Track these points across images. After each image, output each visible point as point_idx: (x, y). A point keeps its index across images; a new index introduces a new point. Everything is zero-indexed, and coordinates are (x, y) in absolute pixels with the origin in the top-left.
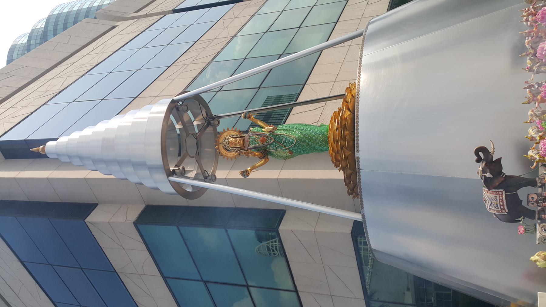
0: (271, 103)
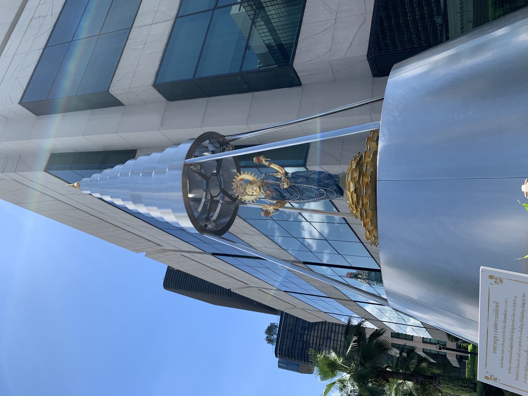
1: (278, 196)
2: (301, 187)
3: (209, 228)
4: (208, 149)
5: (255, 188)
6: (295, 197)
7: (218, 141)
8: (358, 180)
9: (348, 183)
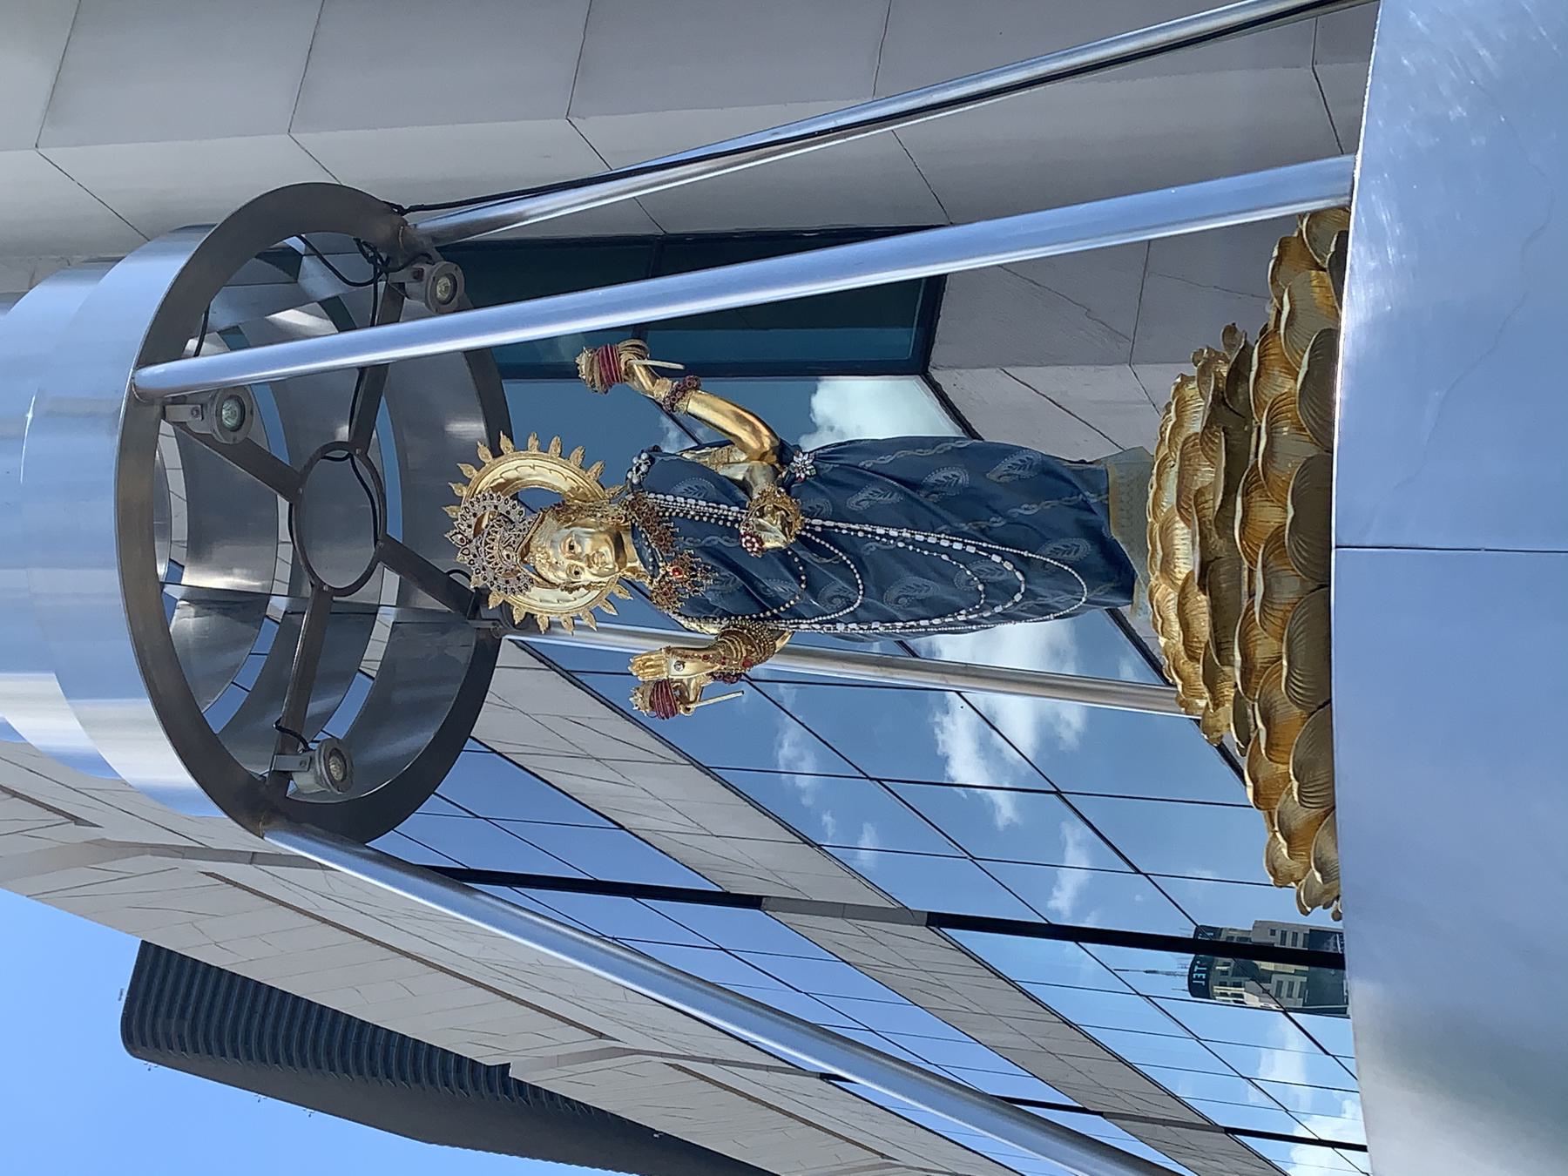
1: (731, 594)
2: (873, 539)
3: (298, 792)
4: (299, 286)
5: (588, 543)
7: (357, 240)
8: (1221, 506)
9: (1157, 526)
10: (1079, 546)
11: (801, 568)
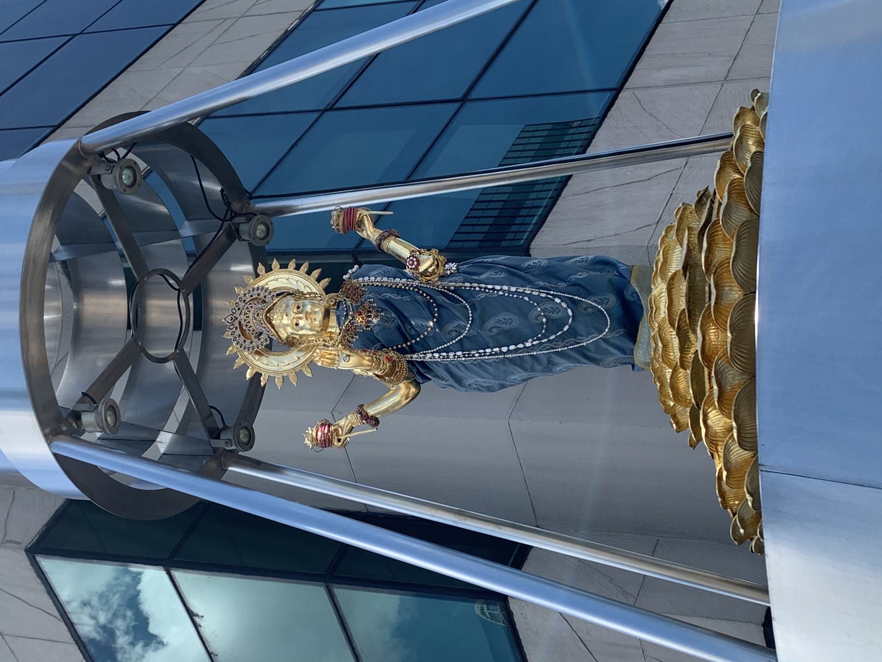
0: (532, 153)
6: (454, 334)
10: (608, 299)
11: (436, 309)
